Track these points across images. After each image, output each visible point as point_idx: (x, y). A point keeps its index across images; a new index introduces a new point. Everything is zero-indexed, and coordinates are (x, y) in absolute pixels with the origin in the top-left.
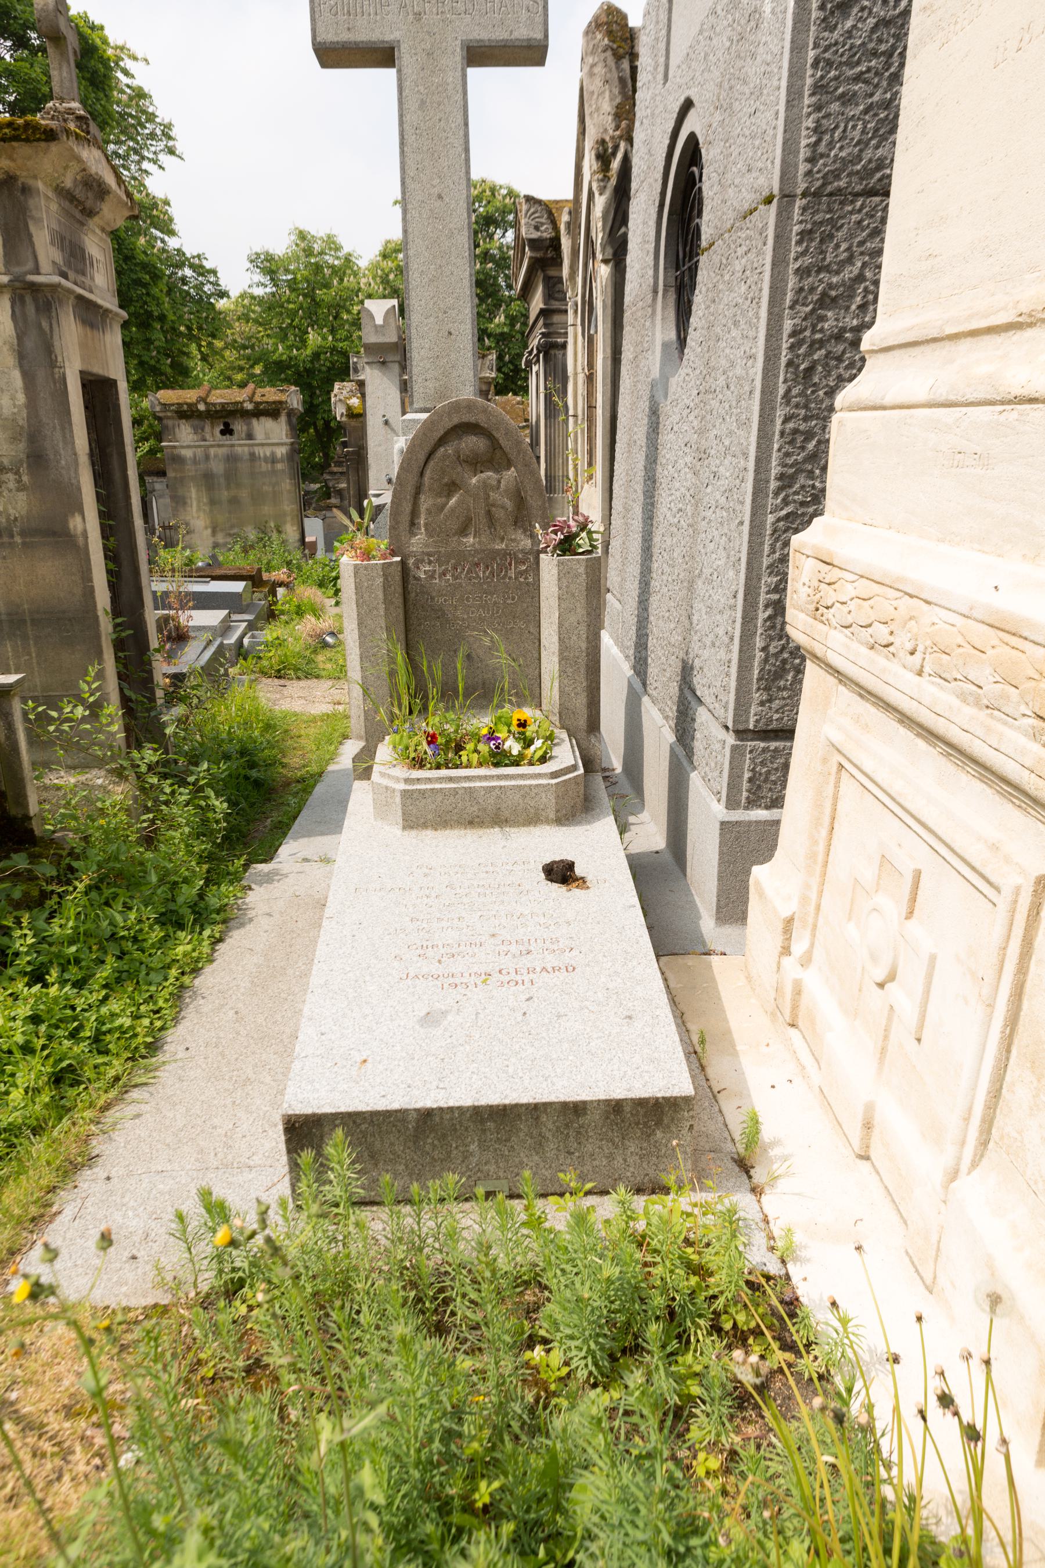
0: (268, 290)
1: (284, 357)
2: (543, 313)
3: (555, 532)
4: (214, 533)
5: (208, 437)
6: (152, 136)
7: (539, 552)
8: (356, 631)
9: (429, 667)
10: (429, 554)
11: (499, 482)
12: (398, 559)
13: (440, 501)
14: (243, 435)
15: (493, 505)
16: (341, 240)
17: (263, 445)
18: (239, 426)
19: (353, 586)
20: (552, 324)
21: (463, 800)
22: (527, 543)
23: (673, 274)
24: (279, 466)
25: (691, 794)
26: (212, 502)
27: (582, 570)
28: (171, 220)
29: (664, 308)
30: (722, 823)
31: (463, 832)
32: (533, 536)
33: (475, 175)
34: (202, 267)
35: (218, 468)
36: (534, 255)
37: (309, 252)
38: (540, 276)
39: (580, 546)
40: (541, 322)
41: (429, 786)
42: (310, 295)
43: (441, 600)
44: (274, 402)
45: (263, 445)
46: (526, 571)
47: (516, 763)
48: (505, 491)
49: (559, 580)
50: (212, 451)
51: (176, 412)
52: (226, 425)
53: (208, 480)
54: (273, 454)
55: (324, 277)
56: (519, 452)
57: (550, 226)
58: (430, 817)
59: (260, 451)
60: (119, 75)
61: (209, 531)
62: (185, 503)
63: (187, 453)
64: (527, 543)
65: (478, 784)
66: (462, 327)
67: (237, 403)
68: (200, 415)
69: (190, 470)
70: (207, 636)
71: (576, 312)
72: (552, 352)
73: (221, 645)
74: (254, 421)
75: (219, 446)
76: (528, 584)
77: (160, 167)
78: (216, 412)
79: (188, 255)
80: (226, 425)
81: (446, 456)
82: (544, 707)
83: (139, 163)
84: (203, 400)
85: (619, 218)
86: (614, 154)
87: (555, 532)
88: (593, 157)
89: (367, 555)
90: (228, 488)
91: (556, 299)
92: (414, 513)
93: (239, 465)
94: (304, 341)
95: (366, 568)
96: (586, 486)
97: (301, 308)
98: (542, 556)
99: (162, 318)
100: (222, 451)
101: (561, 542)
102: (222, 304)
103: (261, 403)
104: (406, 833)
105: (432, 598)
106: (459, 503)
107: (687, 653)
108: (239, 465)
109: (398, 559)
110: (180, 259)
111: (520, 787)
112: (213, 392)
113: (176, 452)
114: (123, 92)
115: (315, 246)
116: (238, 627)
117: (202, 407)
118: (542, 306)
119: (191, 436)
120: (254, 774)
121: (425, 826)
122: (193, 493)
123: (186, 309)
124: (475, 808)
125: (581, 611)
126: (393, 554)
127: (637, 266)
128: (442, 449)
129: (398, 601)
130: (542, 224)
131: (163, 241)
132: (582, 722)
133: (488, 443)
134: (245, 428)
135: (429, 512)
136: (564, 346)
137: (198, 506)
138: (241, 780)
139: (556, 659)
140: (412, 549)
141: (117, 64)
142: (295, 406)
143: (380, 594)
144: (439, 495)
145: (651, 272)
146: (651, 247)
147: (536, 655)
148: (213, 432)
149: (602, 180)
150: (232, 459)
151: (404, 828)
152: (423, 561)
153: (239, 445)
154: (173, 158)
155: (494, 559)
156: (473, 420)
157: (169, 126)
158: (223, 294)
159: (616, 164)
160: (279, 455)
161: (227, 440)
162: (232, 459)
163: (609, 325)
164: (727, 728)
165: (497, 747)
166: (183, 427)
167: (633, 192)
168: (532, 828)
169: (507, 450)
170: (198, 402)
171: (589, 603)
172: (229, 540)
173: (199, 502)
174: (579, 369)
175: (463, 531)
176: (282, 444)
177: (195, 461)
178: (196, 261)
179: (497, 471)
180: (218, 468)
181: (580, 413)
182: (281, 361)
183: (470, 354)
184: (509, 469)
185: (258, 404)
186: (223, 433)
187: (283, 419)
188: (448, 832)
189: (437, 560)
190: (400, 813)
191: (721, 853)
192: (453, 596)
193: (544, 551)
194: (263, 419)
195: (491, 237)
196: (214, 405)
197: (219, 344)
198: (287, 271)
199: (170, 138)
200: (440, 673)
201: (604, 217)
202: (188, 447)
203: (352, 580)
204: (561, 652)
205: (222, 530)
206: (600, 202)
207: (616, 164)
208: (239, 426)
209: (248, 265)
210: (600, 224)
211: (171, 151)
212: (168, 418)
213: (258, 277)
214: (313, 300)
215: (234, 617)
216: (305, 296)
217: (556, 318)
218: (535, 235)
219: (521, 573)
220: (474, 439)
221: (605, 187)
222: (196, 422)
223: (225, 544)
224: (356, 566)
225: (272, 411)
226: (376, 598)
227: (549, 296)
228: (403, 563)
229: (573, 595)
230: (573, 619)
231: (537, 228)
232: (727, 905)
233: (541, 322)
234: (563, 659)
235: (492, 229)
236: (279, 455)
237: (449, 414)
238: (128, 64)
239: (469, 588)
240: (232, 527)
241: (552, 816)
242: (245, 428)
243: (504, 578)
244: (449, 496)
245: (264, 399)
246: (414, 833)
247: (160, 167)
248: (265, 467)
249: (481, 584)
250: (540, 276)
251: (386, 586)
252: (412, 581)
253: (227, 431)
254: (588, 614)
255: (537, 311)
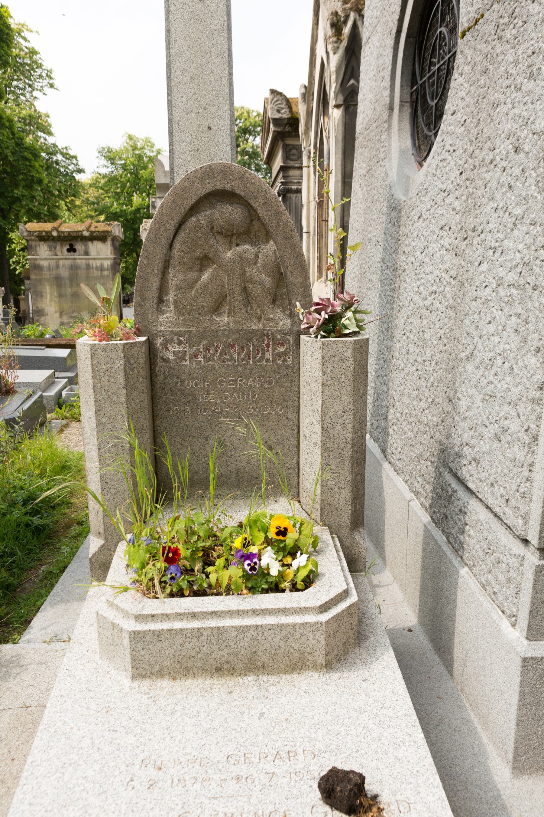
0: (110, 169)
1: (118, 210)
2: (282, 169)
3: (318, 312)
4: (61, 315)
5: (59, 253)
6: (41, 76)
7: (299, 333)
8: (94, 419)
9: (175, 466)
10: (179, 334)
11: (257, 256)
12: (143, 339)
13: (191, 276)
14: (82, 253)
15: (250, 281)
16: (153, 140)
17: (95, 259)
18: (79, 246)
19: (90, 369)
20: (288, 176)
21: (209, 642)
22: (285, 323)
23: (408, 90)
24: (106, 273)
25: (460, 594)
26: (60, 296)
27: (349, 353)
28: (50, 125)
29: (400, 120)
30: (525, 660)
31: (208, 682)
32: (292, 315)
33: (237, 104)
34: (68, 154)
35: (64, 273)
36: (276, 129)
37: (135, 148)
38: (281, 144)
39: (345, 327)
40: (281, 175)
41: (165, 626)
42: (136, 174)
43: (192, 383)
44: (103, 232)
45: (95, 259)
46: (285, 353)
47: (276, 588)
48: (263, 266)
49: (323, 364)
50: (61, 262)
51: (38, 237)
52: (71, 246)
53: (58, 281)
54: (102, 265)
55: (144, 163)
56: (279, 224)
57: (288, 110)
58: (167, 663)
59: (93, 263)
60: (21, 40)
61: (58, 314)
62: (42, 296)
63: (45, 264)
64: (285, 323)
65: (228, 622)
66: (221, 123)
67: (78, 231)
68: (53, 239)
69: (46, 274)
70: (29, 390)
71: (309, 157)
72: (288, 195)
73: (41, 396)
74: (90, 244)
75: (66, 259)
76: (286, 367)
77: (44, 94)
78: (65, 237)
79: (60, 147)
80: (71, 246)
81: (198, 227)
82: (302, 499)
83: (31, 92)
84: (56, 229)
85: (349, 72)
86: (345, 22)
87: (318, 312)
88: (329, 25)
89: (107, 335)
90: (71, 286)
91: (292, 160)
92: (162, 290)
93: (79, 272)
94: (131, 201)
95: (104, 349)
96: (316, 283)
97: (128, 181)
98: (303, 337)
99: (40, 182)
100: (68, 263)
101: (326, 322)
102: (78, 177)
103: (94, 232)
104: (136, 684)
105: (182, 382)
106: (213, 278)
107: (448, 436)
108: (79, 272)
109: (143, 339)
110: (53, 151)
111: (281, 627)
112: (63, 225)
113: (37, 262)
114: (21, 50)
115: (138, 144)
116: (60, 382)
117: (55, 234)
118: (282, 164)
119: (47, 253)
120: (36, 521)
121: (160, 674)
122: (48, 289)
123: (57, 179)
124: (225, 652)
125: (347, 398)
126: (139, 333)
127: (370, 96)
128: (193, 219)
129: (143, 385)
130: (282, 108)
131: (45, 139)
132: (346, 519)
133: (245, 213)
134: (83, 248)
135: (179, 288)
136: (299, 191)
137: (51, 298)
138: (22, 529)
139: (318, 451)
140: (159, 328)
141: (19, 34)
142: (117, 234)
143: (121, 379)
144: (190, 269)
145: (387, 93)
146: (387, 73)
147: (295, 443)
148: (62, 250)
149: (336, 42)
150: (74, 268)
151: (134, 677)
152: (172, 341)
153: (79, 259)
154: (52, 90)
155: (250, 340)
156: (228, 187)
157: (50, 71)
158: (80, 171)
159: (347, 30)
160: (106, 266)
161: (71, 255)
162: (74, 268)
163: (340, 156)
164: (526, 541)
165: (253, 568)
166: (42, 246)
167: (364, 40)
168: (295, 676)
169: (266, 221)
170: (52, 230)
171: (355, 389)
172: (71, 320)
173: (51, 295)
174: (312, 198)
175: (216, 309)
176: (108, 259)
177: (49, 269)
178: (65, 151)
179: (254, 244)
180: (64, 273)
181: (311, 230)
182: (116, 213)
183: (228, 148)
184: (267, 242)
185: (92, 232)
186: (69, 250)
187: (109, 242)
188: (189, 681)
189: (188, 340)
190: (128, 658)
191: (522, 695)
192: (205, 379)
193: (306, 332)
194: (95, 242)
195: (247, 140)
196: (63, 232)
197: (78, 203)
198: (121, 158)
199: (51, 78)
200: (187, 473)
201: (338, 71)
202: (46, 259)
203: (89, 362)
204: (324, 443)
205: (66, 314)
206: (335, 60)
207: (347, 30)
208: (79, 246)
209: (97, 154)
210: (334, 77)
211: (52, 86)
212: (32, 240)
213: (103, 161)
214: (137, 176)
215: (57, 374)
216: (131, 174)
217: (292, 173)
218: (277, 116)
219: (280, 355)
220: (230, 208)
221: (338, 48)
222: (51, 243)
223: (68, 323)
224: (92, 347)
225: (102, 237)
226: (115, 383)
227: (286, 157)
228: (150, 343)
229: (338, 381)
230: (338, 407)
231: (279, 111)
232: (526, 753)
233: (281, 175)
234: (325, 450)
235: (247, 136)
236: (106, 266)
237: (202, 180)
238: (26, 34)
239: (223, 371)
240: (73, 312)
241: (321, 660)
242: (83, 248)
243: (260, 360)
244: (201, 271)
245: (97, 229)
246: (146, 683)
247: (44, 94)
248: (96, 273)
249: (236, 367)
250: (281, 144)
251: (128, 370)
252: (160, 363)
253: (72, 249)
254: (355, 402)
255: (278, 168)
